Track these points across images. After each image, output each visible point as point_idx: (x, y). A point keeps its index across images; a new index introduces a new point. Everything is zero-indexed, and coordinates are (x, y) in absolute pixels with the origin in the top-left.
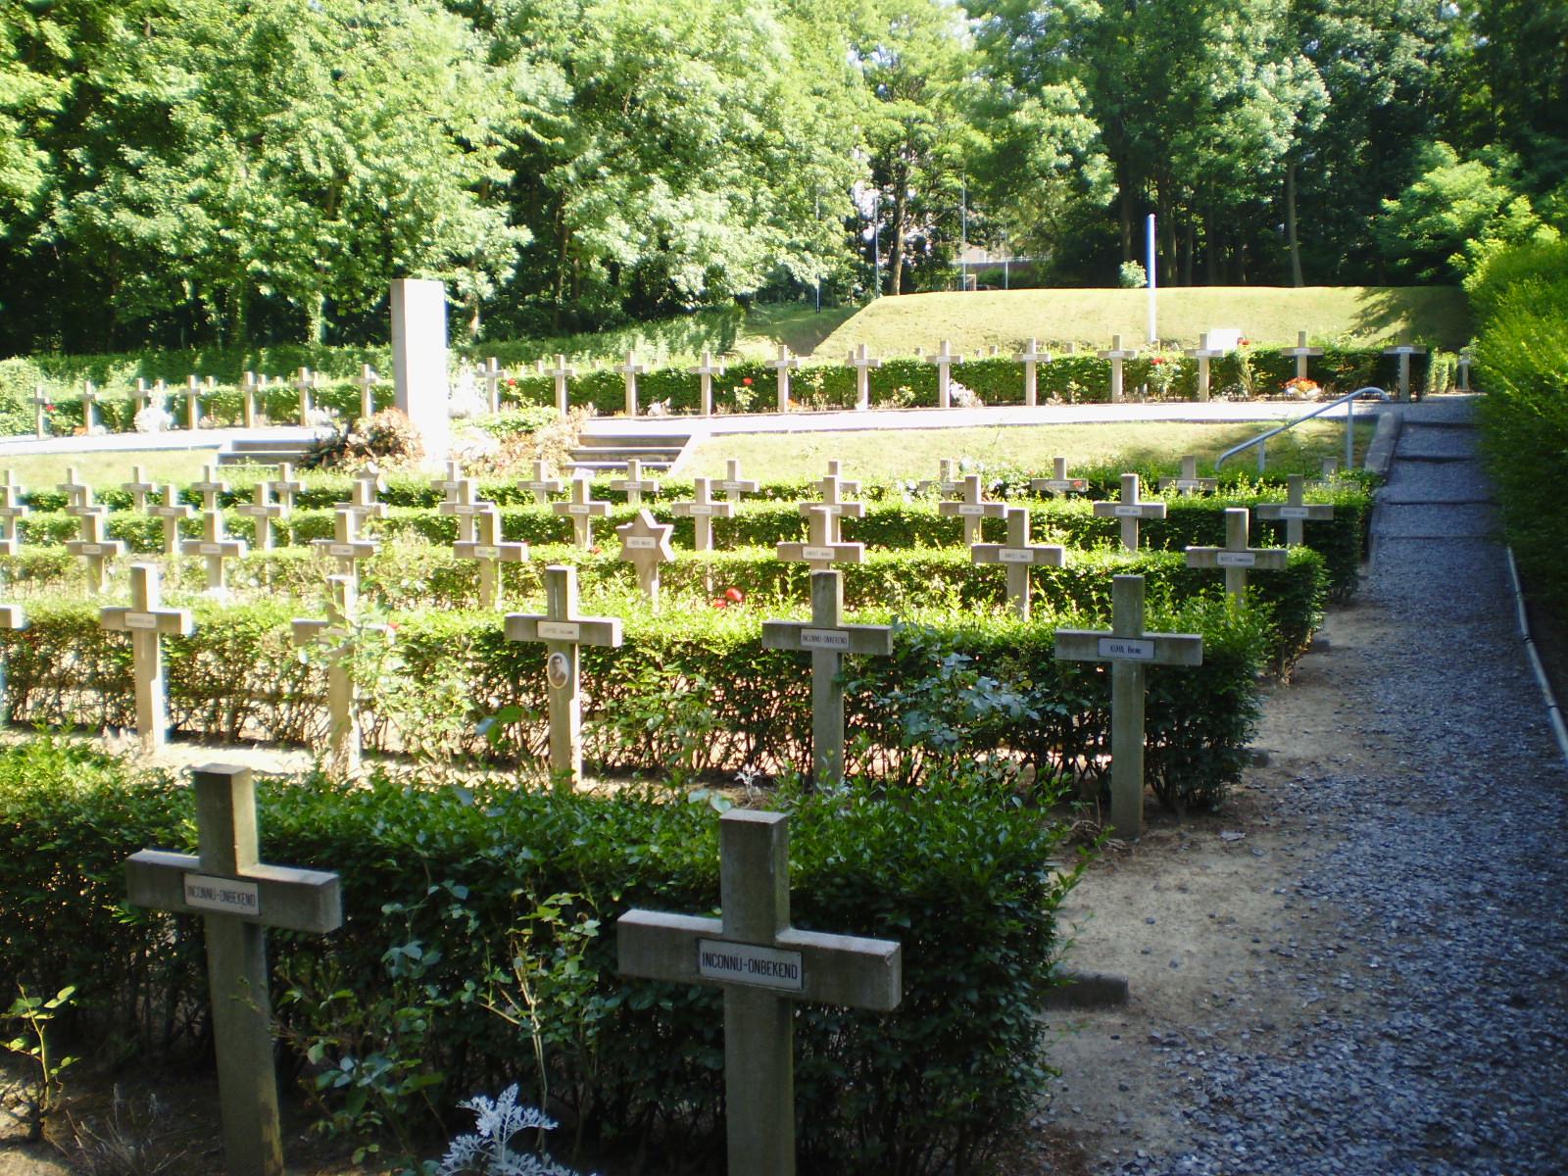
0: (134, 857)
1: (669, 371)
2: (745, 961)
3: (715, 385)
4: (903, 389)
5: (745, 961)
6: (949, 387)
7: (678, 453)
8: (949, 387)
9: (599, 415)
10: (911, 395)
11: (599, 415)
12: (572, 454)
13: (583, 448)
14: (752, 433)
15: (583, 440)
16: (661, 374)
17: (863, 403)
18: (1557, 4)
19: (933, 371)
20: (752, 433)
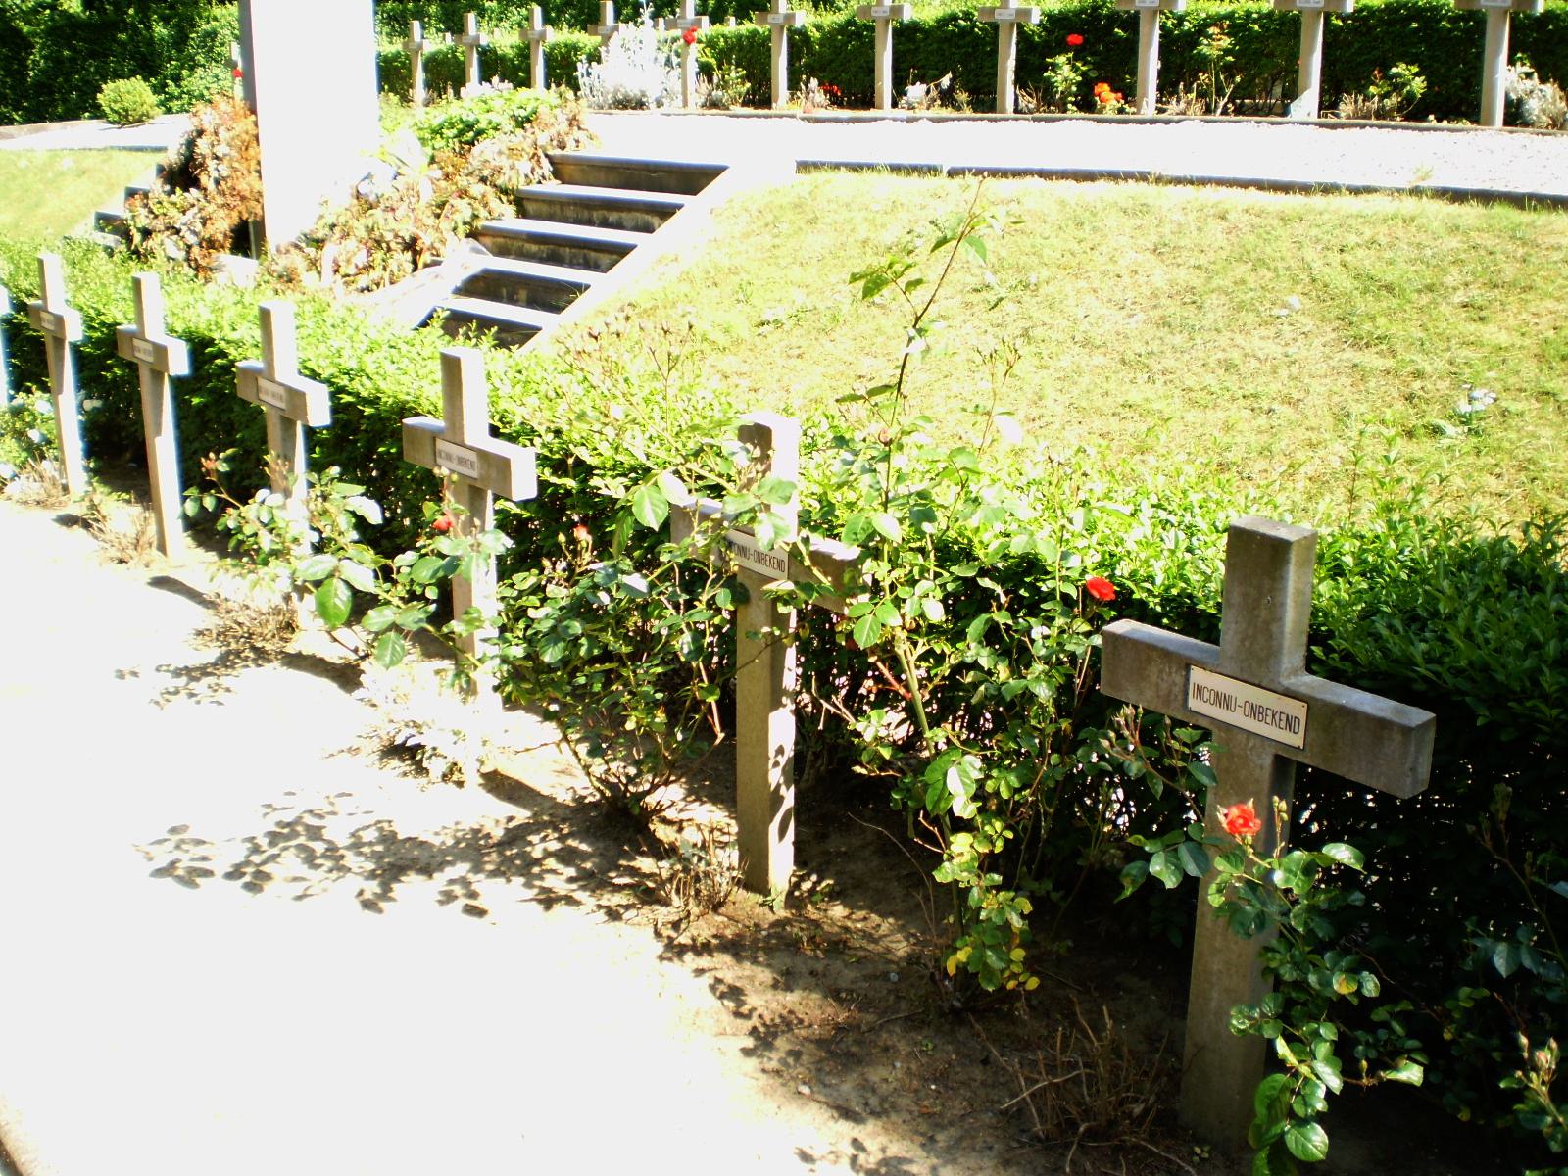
0: (766, 588)
1: (954, 18)
2: (1240, 702)
3: (1024, 38)
4: (1400, 69)
5: (1240, 702)
6: (1507, 77)
7: (622, 251)
8: (1507, 77)
9: (515, 88)
10: (1418, 85)
11: (515, 88)
12: (522, 204)
13: (553, 187)
14: (856, 168)
15: (560, 169)
16: (943, 22)
17: (1308, 101)
18: (1558, 124)
19: (1472, 29)
20: (856, 168)
